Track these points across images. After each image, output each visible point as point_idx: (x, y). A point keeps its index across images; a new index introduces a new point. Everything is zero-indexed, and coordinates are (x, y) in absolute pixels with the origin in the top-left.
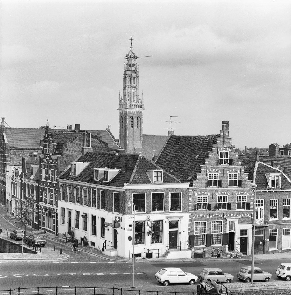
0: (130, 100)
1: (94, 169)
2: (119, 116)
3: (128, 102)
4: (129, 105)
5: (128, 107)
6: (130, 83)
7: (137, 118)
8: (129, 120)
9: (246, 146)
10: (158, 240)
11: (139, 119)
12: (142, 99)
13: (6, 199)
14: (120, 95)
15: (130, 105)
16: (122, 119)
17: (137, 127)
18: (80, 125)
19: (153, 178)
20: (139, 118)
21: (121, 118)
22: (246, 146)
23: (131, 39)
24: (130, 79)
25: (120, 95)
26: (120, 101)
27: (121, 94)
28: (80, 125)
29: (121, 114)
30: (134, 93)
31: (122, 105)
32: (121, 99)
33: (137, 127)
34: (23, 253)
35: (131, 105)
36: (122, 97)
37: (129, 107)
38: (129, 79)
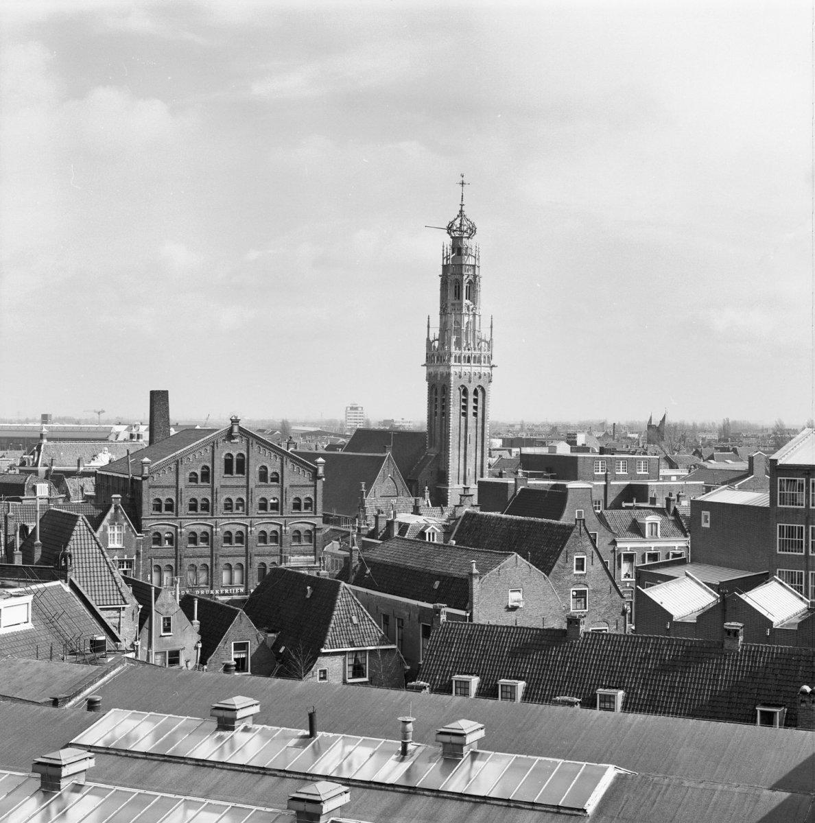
0: (458, 344)
1: (756, 710)
2: (426, 384)
3: (453, 347)
4: (455, 357)
5: (452, 362)
6: (459, 299)
7: (476, 393)
8: (455, 396)
9: (159, 399)
10: (468, 682)
11: (480, 393)
12: (488, 340)
13: (196, 621)
14: (429, 327)
15: (458, 356)
16: (434, 390)
17: (475, 414)
18: (166, 392)
19: (635, 608)
20: (481, 391)
21: (433, 389)
22: (159, 399)
23: (460, 181)
24: (459, 287)
25: (429, 327)
26: (429, 343)
27: (431, 326)
28: (166, 392)
29: (430, 378)
30: (468, 323)
31: (436, 356)
32: (431, 339)
33: (475, 414)
34: (153, 538)
35: (460, 357)
36: (435, 332)
37: (455, 362)
38: (456, 287)
